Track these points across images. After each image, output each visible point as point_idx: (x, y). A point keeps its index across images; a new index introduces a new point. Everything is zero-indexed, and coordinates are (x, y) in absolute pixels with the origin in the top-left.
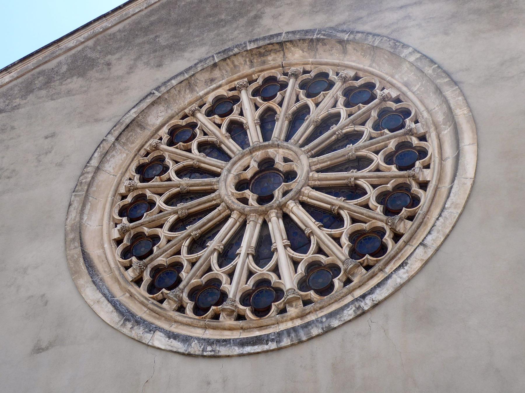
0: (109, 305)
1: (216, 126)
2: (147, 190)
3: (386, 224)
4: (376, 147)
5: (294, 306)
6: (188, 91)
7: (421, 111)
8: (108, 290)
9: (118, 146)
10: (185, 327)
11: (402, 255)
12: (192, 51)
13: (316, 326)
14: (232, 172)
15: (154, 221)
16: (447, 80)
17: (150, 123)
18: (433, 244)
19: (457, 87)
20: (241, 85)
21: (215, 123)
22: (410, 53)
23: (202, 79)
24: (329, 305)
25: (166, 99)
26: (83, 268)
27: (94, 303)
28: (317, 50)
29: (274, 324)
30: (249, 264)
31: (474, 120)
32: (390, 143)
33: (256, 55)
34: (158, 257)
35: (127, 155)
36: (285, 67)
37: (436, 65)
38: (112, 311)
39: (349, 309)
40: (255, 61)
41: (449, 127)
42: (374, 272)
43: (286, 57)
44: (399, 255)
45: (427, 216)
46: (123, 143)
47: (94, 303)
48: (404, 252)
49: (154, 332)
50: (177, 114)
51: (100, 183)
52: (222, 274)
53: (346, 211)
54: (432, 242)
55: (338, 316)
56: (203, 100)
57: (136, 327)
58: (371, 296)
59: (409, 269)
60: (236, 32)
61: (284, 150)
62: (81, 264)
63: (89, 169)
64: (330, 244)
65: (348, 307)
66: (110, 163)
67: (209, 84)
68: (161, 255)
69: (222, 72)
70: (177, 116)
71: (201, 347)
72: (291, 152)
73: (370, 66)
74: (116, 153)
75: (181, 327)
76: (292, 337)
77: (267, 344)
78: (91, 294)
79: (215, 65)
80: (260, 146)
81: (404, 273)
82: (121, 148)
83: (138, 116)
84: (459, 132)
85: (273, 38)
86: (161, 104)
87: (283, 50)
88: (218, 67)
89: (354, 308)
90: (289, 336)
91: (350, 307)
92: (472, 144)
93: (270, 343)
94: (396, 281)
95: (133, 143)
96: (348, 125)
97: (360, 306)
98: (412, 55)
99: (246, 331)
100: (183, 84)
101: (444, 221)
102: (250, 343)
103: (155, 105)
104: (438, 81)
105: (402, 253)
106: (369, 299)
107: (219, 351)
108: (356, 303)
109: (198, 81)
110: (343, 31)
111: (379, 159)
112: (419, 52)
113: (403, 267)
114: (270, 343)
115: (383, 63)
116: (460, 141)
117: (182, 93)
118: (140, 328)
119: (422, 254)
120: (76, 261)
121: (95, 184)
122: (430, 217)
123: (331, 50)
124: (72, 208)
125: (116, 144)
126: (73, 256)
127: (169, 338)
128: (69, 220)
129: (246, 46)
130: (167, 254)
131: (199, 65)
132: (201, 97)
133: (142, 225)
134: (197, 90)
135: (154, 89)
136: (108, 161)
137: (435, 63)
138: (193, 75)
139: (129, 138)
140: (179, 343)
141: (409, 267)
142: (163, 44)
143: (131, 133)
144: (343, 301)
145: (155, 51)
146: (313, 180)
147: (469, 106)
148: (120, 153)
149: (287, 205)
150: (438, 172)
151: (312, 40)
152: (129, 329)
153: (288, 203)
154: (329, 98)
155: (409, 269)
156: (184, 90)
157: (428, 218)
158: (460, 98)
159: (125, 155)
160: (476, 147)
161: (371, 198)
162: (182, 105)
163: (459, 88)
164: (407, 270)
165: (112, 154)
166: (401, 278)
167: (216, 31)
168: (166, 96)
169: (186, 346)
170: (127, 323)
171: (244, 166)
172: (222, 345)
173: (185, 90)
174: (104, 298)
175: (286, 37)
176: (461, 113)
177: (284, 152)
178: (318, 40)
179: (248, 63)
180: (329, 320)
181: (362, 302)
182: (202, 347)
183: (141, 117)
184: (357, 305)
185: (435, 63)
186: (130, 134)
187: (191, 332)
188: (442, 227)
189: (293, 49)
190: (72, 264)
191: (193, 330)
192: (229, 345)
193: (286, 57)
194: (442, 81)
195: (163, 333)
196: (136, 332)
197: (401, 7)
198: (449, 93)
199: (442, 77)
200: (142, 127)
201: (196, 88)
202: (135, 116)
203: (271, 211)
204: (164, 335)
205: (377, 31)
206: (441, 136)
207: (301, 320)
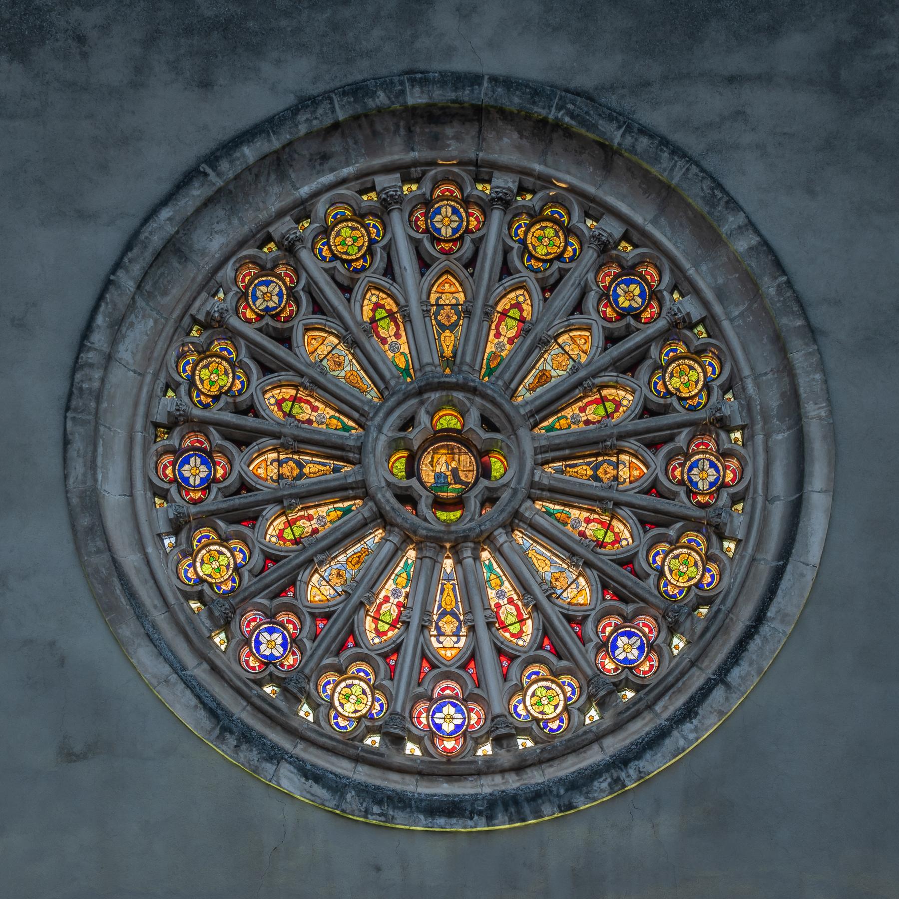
0: (188, 693)
1: (334, 285)
2: (212, 429)
3: (664, 617)
4: (655, 437)
5: (505, 746)
6: (273, 177)
7: (744, 375)
8: (171, 651)
9: (140, 303)
10: (319, 752)
11: (684, 683)
12: (278, 62)
13: (550, 801)
14: (385, 430)
15: (237, 510)
16: (799, 323)
17: (197, 247)
18: (740, 685)
19: (816, 347)
20: (392, 196)
21: (333, 278)
22: (740, 227)
23: (305, 152)
24: (563, 755)
25: (231, 192)
26: (123, 600)
27: (159, 683)
28: (551, 141)
29: (471, 775)
30: (425, 647)
31: (833, 435)
32: (680, 433)
33: (422, 117)
34: (255, 596)
35: (156, 322)
36: (481, 166)
37: (784, 278)
38: (196, 707)
39: (601, 780)
40: (418, 130)
41: (789, 429)
42: (638, 710)
43: (484, 139)
44: (680, 684)
45: (731, 615)
46: (148, 292)
47: (159, 683)
48: (689, 679)
49: (278, 763)
50: (254, 236)
51: (113, 390)
52: (377, 658)
53: (595, 573)
54: (739, 680)
55: (584, 789)
56: (305, 208)
57: (244, 747)
58: (637, 763)
59: (699, 725)
60: (377, 33)
61: (485, 403)
62: (118, 592)
63: (90, 356)
64: (560, 628)
65: (601, 776)
66: (127, 340)
67: (318, 167)
68: (259, 594)
69: (347, 143)
70: (252, 241)
71: (362, 804)
72: (498, 412)
73: (654, 222)
74: (137, 317)
75: (312, 750)
76: (511, 813)
77: (471, 819)
78: (144, 655)
79: (336, 126)
80: (439, 383)
81: (691, 731)
82: (143, 304)
83: (177, 232)
84: (807, 458)
85: (463, 88)
86: (219, 202)
87: (479, 120)
88: (340, 130)
89: (609, 780)
90: (506, 810)
91: (604, 777)
92: (826, 491)
93: (476, 817)
94: (677, 742)
95: (165, 293)
96: (605, 370)
97: (618, 779)
98: (742, 233)
99: (425, 778)
100: (267, 161)
101: (763, 644)
102: (443, 811)
103: (210, 206)
104: (784, 321)
105: (685, 679)
106: (634, 767)
107: (393, 817)
108: (613, 771)
109: (296, 156)
110: (614, 116)
111: (658, 468)
112: (757, 231)
113: (691, 719)
114: (476, 817)
115: (681, 225)
116: (806, 479)
117: (263, 179)
118: (251, 751)
119: (722, 701)
120: (105, 583)
121: (106, 393)
122: (735, 618)
123: (581, 153)
124: (72, 453)
125: (137, 297)
126: (97, 571)
127: (307, 779)
128: (71, 480)
129: (403, 92)
130: (270, 591)
131: (302, 117)
132: (303, 202)
133: (213, 515)
134: (293, 176)
135: (205, 162)
136: (124, 336)
137: (784, 273)
138: (290, 144)
139: (157, 282)
140: (324, 791)
141: (700, 722)
142: (209, 13)
143: (162, 270)
144: (585, 752)
145: (189, 31)
146: (539, 489)
147: (829, 401)
148: (144, 317)
149: (492, 537)
150: (759, 528)
151: (544, 121)
152: (232, 747)
153: (496, 533)
154: (573, 288)
155: (699, 725)
156: (266, 172)
157: (732, 619)
158: (818, 376)
159: (151, 323)
160: (830, 499)
161: (640, 553)
162: (263, 216)
163: (819, 351)
164: (696, 727)
165: (130, 320)
166: (685, 739)
167: (328, 14)
168: (231, 187)
169: (337, 798)
170: (227, 735)
171: (405, 418)
172: (399, 808)
173: (269, 174)
174: (175, 676)
175: (490, 93)
176: (815, 413)
177: (484, 405)
178: (557, 125)
179: (402, 132)
180: (569, 793)
181: (622, 770)
182: (364, 805)
183: (180, 235)
184: (615, 775)
185: (784, 273)
186: (159, 272)
187: (333, 764)
188: (758, 656)
189: (500, 123)
190: (100, 589)
191: (334, 759)
192: (408, 810)
193: (484, 139)
194: (791, 323)
195: (295, 767)
196: (245, 756)
197: (732, 80)
198: (800, 356)
199: (793, 312)
200: (184, 258)
201: (291, 171)
202: (171, 229)
203: (465, 544)
204: (296, 771)
205: (678, 137)
206: (770, 444)
207: (517, 775)
